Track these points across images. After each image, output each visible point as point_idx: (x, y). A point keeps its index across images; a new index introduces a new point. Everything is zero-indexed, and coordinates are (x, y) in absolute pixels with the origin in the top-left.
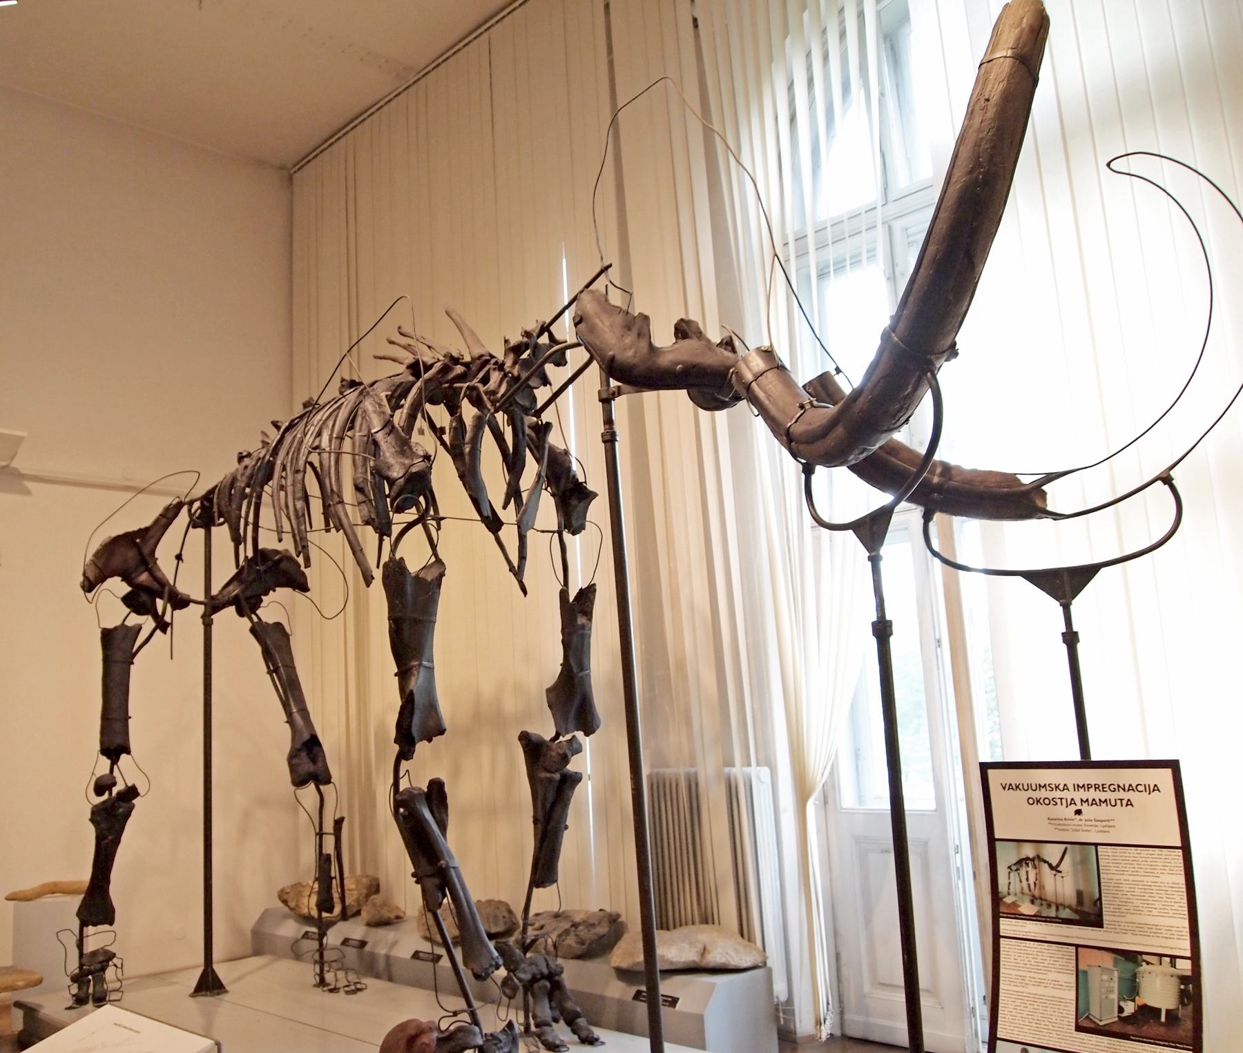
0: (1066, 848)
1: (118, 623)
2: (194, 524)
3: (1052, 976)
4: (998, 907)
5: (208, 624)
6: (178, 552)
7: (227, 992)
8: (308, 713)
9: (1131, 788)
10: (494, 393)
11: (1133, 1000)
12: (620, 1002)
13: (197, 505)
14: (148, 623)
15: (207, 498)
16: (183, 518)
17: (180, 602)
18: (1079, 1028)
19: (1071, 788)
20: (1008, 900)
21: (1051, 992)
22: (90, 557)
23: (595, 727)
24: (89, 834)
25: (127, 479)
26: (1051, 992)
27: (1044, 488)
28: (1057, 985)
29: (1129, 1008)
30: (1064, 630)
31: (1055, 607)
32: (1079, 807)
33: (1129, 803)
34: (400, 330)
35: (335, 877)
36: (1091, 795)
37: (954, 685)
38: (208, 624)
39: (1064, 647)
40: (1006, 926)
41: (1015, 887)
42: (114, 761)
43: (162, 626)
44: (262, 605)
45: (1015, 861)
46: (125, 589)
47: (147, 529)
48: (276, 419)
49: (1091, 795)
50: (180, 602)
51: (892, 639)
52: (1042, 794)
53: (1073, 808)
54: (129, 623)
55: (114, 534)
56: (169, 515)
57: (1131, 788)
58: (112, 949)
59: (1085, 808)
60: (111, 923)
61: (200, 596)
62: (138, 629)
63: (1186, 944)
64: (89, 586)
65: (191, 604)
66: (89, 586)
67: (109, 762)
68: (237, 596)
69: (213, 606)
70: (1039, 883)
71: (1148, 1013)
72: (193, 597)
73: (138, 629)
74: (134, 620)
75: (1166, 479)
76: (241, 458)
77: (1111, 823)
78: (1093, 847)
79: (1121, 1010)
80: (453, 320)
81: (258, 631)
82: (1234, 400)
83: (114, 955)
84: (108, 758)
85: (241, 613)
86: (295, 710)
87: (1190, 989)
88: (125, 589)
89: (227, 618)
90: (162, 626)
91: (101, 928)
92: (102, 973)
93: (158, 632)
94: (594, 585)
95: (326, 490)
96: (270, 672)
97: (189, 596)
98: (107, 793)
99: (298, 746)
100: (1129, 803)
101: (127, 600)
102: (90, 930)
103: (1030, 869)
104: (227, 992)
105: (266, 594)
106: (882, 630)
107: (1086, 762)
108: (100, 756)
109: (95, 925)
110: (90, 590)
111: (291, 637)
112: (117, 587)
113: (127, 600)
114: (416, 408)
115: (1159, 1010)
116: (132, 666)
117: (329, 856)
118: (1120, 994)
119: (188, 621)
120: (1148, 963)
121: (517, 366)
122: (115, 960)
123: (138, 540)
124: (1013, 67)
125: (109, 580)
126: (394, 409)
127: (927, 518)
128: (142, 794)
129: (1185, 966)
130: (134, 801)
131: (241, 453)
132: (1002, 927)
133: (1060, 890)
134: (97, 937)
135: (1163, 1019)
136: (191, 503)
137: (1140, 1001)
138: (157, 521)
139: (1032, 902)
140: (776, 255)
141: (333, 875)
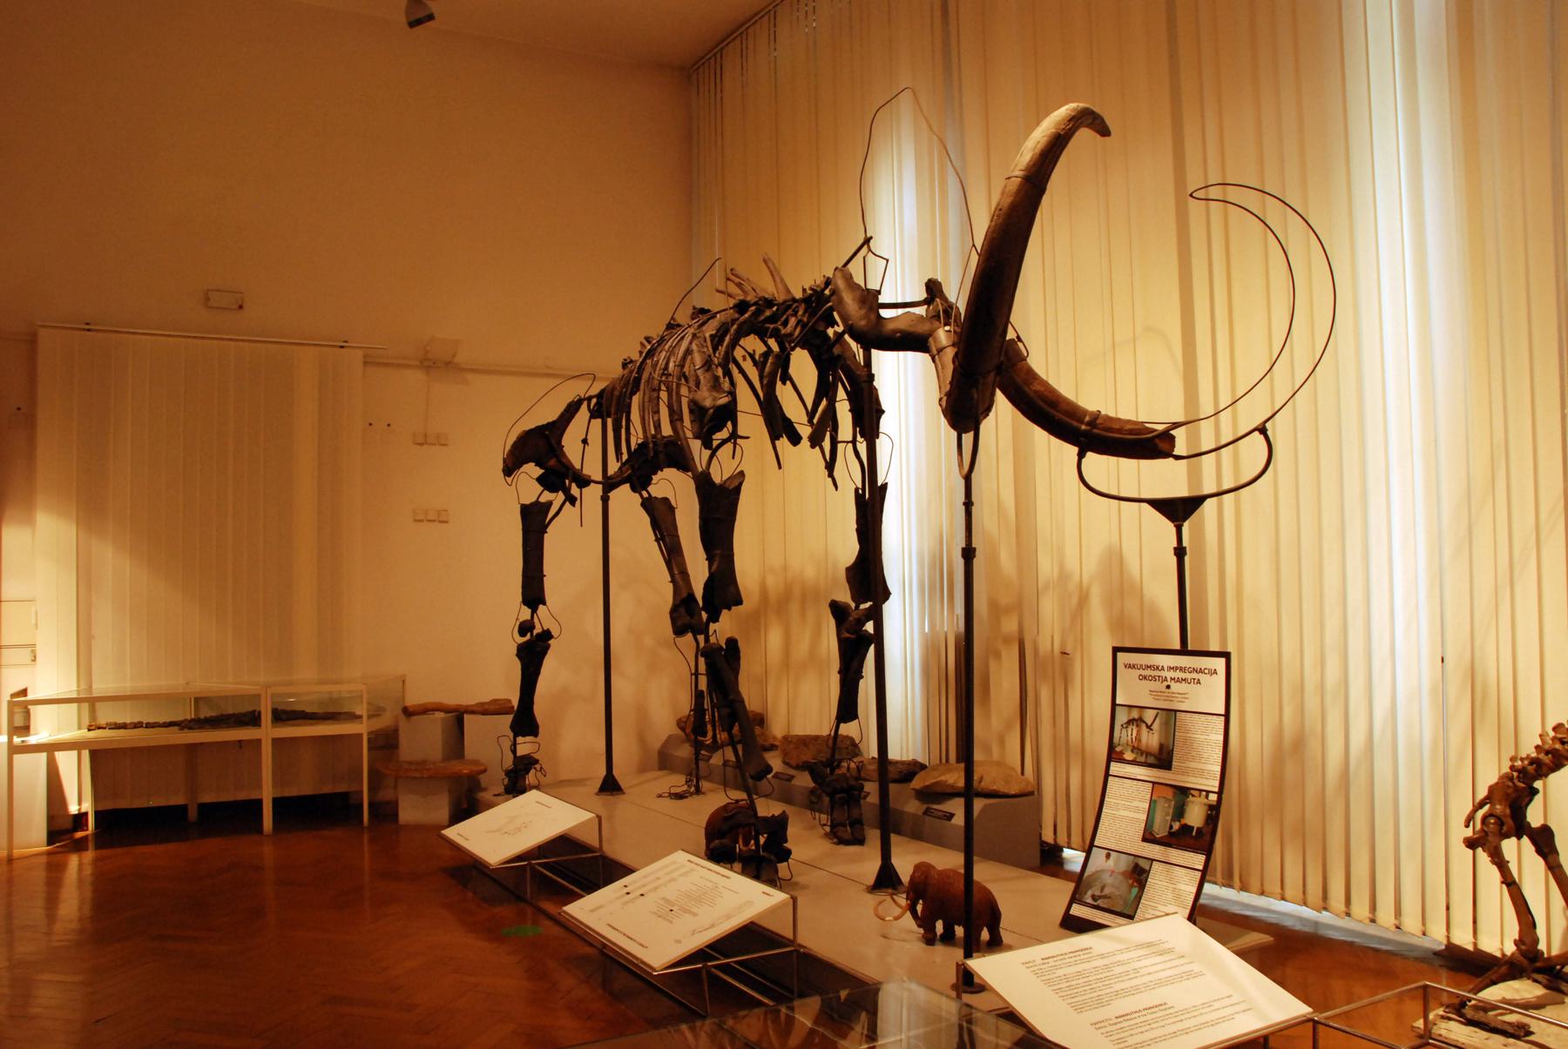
0: (1158, 714)
1: (534, 499)
2: (594, 414)
3: (1136, 803)
4: (1113, 755)
5: (605, 500)
6: (584, 437)
7: (624, 793)
8: (688, 575)
9: (1201, 671)
10: (791, 335)
11: (1179, 821)
12: (915, 815)
13: (594, 401)
14: (560, 497)
15: (600, 396)
16: (583, 412)
17: (584, 482)
18: (1145, 839)
19: (1166, 669)
20: (1118, 749)
22: (508, 447)
24: (516, 667)
25: (547, 367)
27: (1172, 432)
28: (1137, 810)
29: (1176, 826)
30: (1176, 546)
31: (1169, 527)
32: (1169, 683)
34: (734, 272)
35: (708, 710)
36: (1178, 674)
37: (143, 748)
38: (605, 500)
39: (1175, 558)
40: (1116, 768)
41: (1124, 740)
42: (534, 610)
43: (572, 500)
44: (653, 482)
45: (1126, 721)
46: (539, 471)
47: (554, 423)
48: (649, 335)
49: (1178, 674)
50: (584, 482)
53: (1166, 683)
54: (543, 499)
55: (527, 428)
56: (571, 410)
57: (1201, 671)
58: (536, 756)
59: (1173, 684)
60: (536, 735)
61: (599, 477)
62: (550, 504)
63: (1217, 783)
64: (510, 468)
65: (592, 484)
66: (510, 468)
67: (530, 611)
68: (629, 476)
69: (609, 484)
70: (1138, 738)
71: (1186, 829)
72: (593, 478)
73: (550, 504)
74: (547, 496)
75: (1262, 430)
76: (624, 365)
77: (1186, 696)
78: (1173, 713)
79: (1171, 827)
80: (768, 268)
81: (649, 505)
82: (1249, 391)
83: (537, 761)
84: (529, 608)
85: (634, 489)
86: (676, 572)
87: (1213, 813)
88: (539, 471)
89: (624, 497)
90: (572, 500)
91: (528, 739)
92: (524, 773)
93: (567, 503)
94: (887, 483)
96: (657, 540)
97: (590, 477)
98: (529, 635)
99: (678, 602)
100: (1199, 682)
101: (540, 480)
102: (520, 739)
103: (1134, 727)
104: (624, 793)
105: (655, 473)
108: (523, 606)
109: (524, 736)
110: (509, 475)
111: (676, 510)
112: (532, 470)
113: (540, 480)
114: (734, 343)
115: (1193, 827)
116: (546, 535)
117: (702, 691)
118: (1173, 816)
119: (593, 493)
120: (1193, 796)
121: (807, 315)
122: (538, 766)
123: (547, 433)
124: (1020, 185)
125: (525, 466)
126: (715, 349)
127: (1081, 456)
128: (555, 636)
129: (1213, 797)
130: (550, 642)
131: (625, 360)
132: (1111, 768)
133: (1150, 742)
134: (525, 746)
135: (1194, 834)
136: (589, 399)
138: (562, 416)
139: (1132, 751)
140: (974, 245)
141: (706, 707)
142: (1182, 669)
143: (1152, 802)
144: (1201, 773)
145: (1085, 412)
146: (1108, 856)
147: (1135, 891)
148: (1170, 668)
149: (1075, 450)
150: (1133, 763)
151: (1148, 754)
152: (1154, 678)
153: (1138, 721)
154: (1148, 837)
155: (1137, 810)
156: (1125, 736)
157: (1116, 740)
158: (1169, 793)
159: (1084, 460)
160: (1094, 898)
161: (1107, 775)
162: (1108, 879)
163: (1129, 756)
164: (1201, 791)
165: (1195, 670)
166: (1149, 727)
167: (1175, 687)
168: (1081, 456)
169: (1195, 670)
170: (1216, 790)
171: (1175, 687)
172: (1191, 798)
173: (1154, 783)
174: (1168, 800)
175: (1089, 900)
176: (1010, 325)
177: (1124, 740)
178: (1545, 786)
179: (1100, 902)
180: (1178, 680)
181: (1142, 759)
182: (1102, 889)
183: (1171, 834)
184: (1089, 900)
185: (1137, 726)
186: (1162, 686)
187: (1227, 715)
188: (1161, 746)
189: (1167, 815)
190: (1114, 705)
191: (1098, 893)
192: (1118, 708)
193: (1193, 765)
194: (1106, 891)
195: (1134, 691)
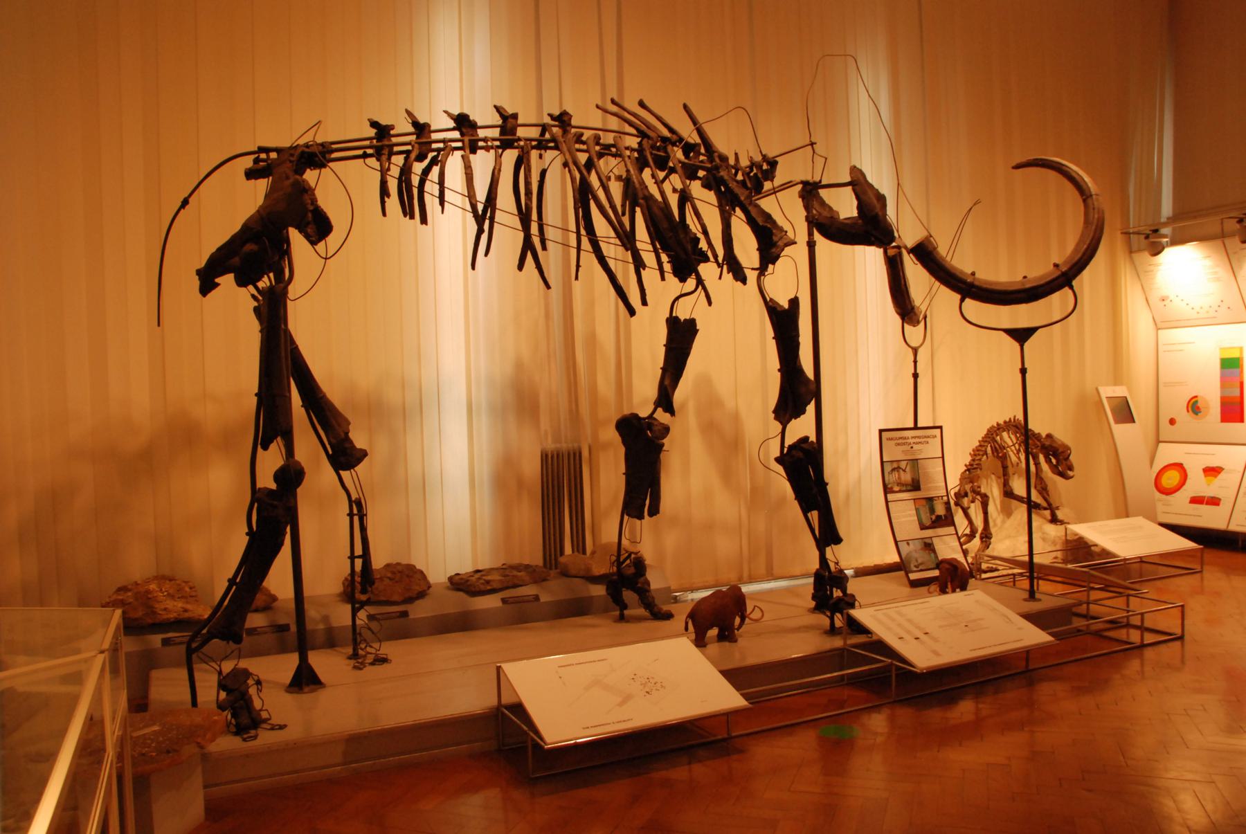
3: (909, 512)
4: (887, 490)
9: (928, 437)
18: (922, 529)
20: (889, 486)
21: (909, 519)
23: (1077, 537)
26: (909, 519)
28: (910, 515)
29: (934, 517)
31: (1016, 345)
33: (928, 443)
39: (227, 584)
40: (890, 497)
41: (891, 481)
51: (1027, 375)
52: (900, 441)
53: (910, 446)
57: (928, 437)
70: (899, 478)
71: (939, 517)
95: (618, 213)
100: (928, 443)
103: (896, 472)
106: (916, 376)
107: (1158, 442)
127: (962, 300)
137: (936, 514)
142: (919, 437)
143: (917, 510)
144: (936, 488)
145: (1177, 241)
146: (908, 544)
147: (932, 555)
148: (912, 437)
149: (958, 297)
150: (900, 491)
151: (906, 485)
152: (904, 444)
153: (898, 469)
154: (923, 527)
155: (910, 515)
156: (892, 478)
157: (887, 482)
158: (924, 502)
159: (963, 304)
160: (916, 566)
161: (887, 502)
162: (915, 555)
163: (896, 488)
164: (938, 497)
165: (925, 437)
166: (904, 471)
167: (916, 447)
168: (962, 300)
169: (925, 437)
170: (945, 494)
171: (916, 447)
172: (935, 502)
173: (914, 499)
174: (923, 506)
175: (915, 569)
176: (620, 244)
177: (891, 481)
178: (752, 599)
179: (921, 568)
180: (917, 443)
181: (904, 488)
182: (917, 561)
183: (933, 522)
184: (915, 569)
185: (898, 471)
186: (907, 448)
187: (943, 457)
188: (913, 479)
189: (927, 513)
190: (882, 462)
191: (916, 564)
192: (885, 464)
193: (930, 485)
194: (920, 561)
195: (893, 453)
